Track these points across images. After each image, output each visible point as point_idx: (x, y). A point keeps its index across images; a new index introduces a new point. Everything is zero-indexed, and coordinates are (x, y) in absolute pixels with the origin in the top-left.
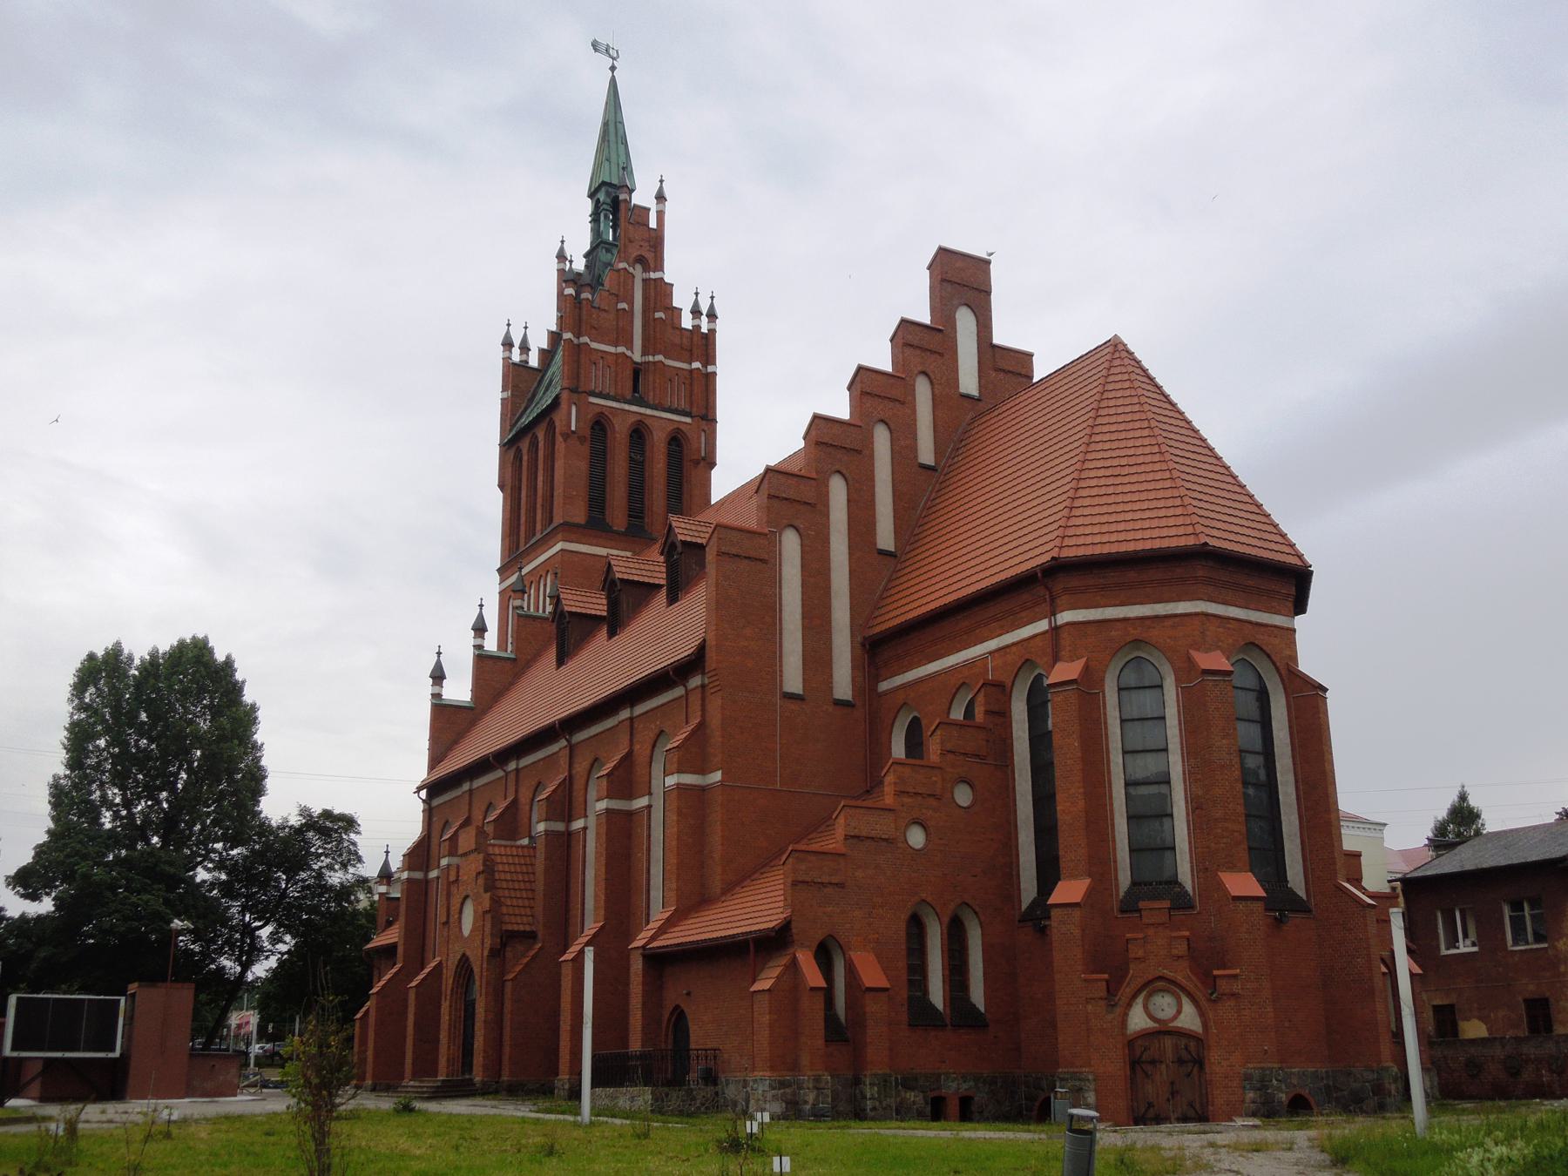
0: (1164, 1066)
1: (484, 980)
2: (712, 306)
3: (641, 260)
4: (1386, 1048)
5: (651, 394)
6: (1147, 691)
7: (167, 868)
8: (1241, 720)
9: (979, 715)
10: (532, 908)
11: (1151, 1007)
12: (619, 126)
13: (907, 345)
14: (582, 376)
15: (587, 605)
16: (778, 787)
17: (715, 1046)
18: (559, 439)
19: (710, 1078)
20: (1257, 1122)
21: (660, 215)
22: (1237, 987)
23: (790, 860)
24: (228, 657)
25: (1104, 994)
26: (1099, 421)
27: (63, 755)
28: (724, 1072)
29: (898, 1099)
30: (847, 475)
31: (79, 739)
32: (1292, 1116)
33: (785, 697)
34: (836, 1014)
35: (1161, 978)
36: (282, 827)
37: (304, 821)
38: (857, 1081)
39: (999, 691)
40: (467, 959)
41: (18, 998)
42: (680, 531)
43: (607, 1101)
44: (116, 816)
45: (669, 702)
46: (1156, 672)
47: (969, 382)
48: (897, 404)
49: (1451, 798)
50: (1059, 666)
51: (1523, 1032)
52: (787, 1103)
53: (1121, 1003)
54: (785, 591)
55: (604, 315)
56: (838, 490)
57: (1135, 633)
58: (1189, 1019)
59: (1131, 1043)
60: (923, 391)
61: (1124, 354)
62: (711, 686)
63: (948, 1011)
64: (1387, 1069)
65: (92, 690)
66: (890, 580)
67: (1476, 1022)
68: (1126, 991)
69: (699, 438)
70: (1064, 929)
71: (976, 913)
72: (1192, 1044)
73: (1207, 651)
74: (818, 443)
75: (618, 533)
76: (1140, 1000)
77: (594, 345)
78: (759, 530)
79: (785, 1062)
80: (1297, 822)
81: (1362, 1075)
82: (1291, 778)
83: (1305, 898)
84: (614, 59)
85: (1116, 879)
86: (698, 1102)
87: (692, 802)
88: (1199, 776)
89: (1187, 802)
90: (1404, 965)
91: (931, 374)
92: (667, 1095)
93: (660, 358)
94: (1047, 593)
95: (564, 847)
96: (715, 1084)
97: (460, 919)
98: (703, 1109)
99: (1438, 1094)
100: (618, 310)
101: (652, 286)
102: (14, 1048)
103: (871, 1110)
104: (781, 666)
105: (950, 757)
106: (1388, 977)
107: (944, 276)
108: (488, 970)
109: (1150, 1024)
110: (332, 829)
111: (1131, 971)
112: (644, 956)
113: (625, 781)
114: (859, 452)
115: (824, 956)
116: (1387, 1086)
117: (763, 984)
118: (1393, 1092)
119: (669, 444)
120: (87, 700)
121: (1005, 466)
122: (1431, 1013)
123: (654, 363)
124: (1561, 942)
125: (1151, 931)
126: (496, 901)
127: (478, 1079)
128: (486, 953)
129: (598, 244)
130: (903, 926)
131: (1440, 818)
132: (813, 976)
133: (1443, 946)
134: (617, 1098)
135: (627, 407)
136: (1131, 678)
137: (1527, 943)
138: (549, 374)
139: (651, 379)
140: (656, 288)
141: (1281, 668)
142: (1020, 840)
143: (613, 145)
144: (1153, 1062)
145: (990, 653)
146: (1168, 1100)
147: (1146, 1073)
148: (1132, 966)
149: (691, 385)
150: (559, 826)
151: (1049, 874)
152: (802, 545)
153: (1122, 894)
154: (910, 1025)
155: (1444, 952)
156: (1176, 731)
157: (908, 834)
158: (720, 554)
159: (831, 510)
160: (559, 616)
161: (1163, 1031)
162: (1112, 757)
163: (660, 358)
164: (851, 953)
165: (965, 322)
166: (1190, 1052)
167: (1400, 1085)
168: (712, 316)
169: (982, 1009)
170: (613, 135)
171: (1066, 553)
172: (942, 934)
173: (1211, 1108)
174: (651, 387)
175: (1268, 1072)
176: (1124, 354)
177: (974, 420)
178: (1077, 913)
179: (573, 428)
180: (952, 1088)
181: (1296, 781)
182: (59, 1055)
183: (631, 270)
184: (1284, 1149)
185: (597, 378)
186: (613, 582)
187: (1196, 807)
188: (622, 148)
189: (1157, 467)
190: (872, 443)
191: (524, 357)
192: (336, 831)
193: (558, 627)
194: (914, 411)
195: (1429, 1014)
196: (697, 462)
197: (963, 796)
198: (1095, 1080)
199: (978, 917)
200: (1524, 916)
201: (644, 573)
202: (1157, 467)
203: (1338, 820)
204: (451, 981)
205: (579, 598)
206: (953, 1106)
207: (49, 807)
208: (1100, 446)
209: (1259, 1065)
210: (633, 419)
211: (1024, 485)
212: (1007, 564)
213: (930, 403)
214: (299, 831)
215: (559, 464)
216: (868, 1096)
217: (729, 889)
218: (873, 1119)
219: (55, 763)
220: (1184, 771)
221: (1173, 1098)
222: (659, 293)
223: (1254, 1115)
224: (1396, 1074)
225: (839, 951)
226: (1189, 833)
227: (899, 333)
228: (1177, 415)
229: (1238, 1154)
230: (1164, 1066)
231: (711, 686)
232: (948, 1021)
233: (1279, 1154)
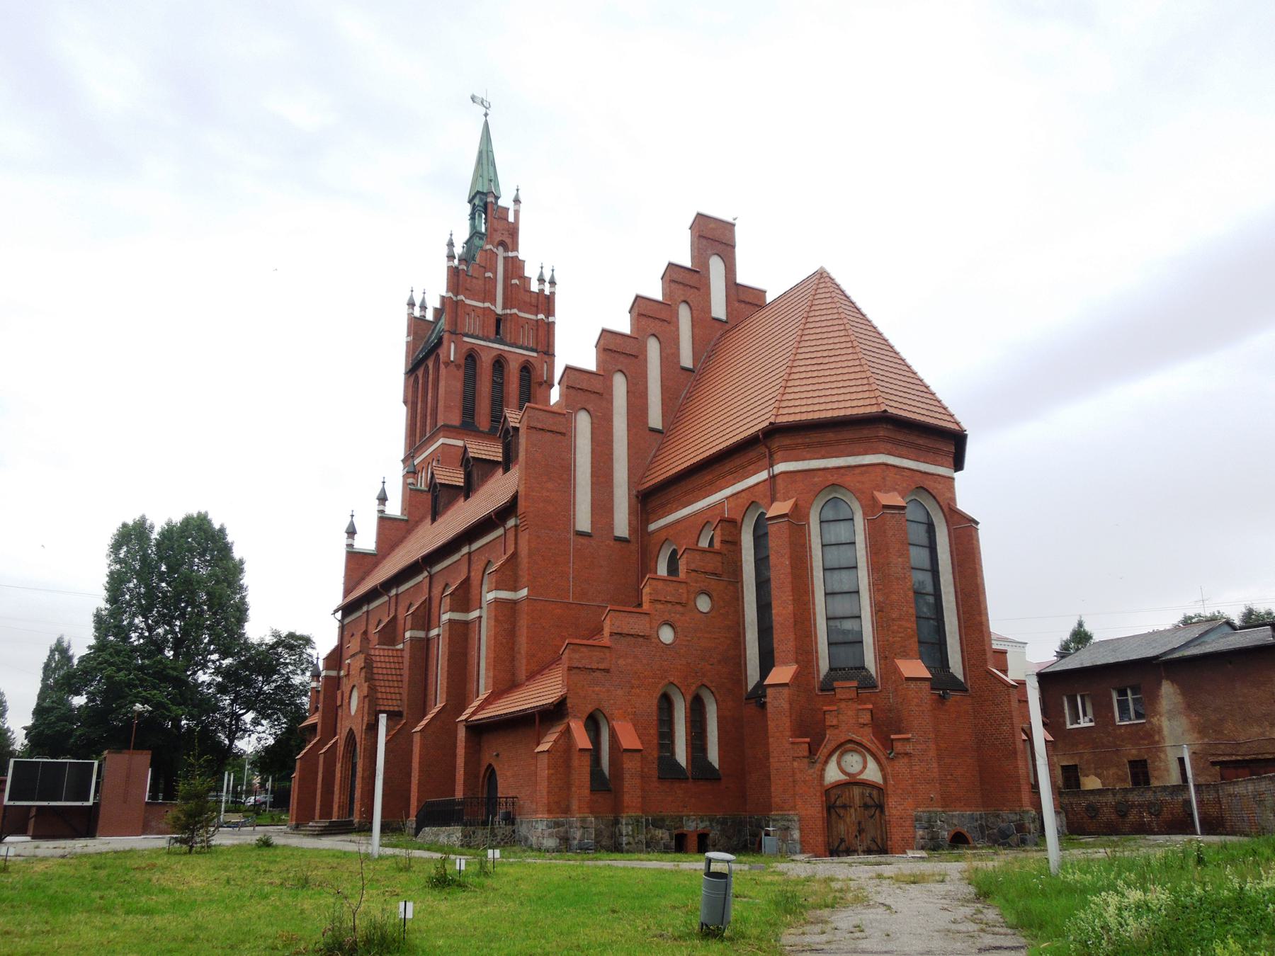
0: (853, 810)
1: (363, 747)
2: (553, 276)
3: (502, 244)
4: (1026, 797)
5: (508, 336)
6: (842, 523)
7: (171, 672)
8: (914, 545)
9: (717, 545)
10: (400, 694)
11: (843, 764)
12: (490, 153)
13: (673, 281)
14: (459, 323)
15: (453, 479)
16: (571, 601)
17: (514, 795)
18: (442, 366)
19: (510, 819)
20: (923, 854)
21: (517, 213)
22: (909, 748)
23: (567, 651)
24: (222, 526)
25: (806, 754)
26: (808, 326)
27: (105, 594)
28: (520, 815)
29: (649, 836)
30: (627, 373)
31: (116, 584)
32: (953, 849)
33: (577, 534)
34: (602, 770)
35: (850, 741)
36: (260, 645)
37: (275, 640)
38: (616, 822)
39: (731, 526)
40: (353, 732)
41: (15, 762)
42: (512, 420)
43: (432, 837)
44: (141, 636)
45: (494, 540)
46: (849, 509)
47: (719, 309)
48: (666, 324)
49: (1073, 625)
50: (776, 505)
51: (1129, 785)
52: (560, 839)
53: (819, 760)
54: (578, 456)
55: (474, 280)
56: (620, 385)
57: (833, 479)
58: (872, 773)
59: (828, 791)
60: (684, 315)
61: (827, 280)
62: (522, 525)
63: (690, 768)
64: (1027, 812)
65: (125, 549)
66: (658, 450)
67: (1093, 777)
68: (824, 751)
69: (542, 367)
70: (777, 703)
71: (712, 693)
72: (875, 793)
73: (887, 492)
74: (605, 350)
75: (482, 432)
76: (834, 758)
77: (468, 302)
78: (559, 411)
79: (559, 806)
80: (957, 623)
81: (262, 785)
82: (952, 590)
83: (963, 680)
84: (486, 108)
85: (818, 665)
86: (499, 838)
87: (506, 610)
88: (881, 587)
89: (871, 606)
90: (1040, 735)
91: (690, 302)
92: (474, 833)
93: (515, 311)
94: (767, 450)
95: (423, 648)
96: (513, 824)
97: (349, 702)
98: (502, 844)
99: (1066, 831)
100: (485, 278)
101: (510, 262)
102: (10, 799)
103: (626, 844)
104: (574, 511)
105: (694, 574)
106: (1028, 743)
107: (701, 233)
108: (365, 739)
109: (843, 777)
110: (296, 646)
111: (827, 736)
112: (467, 727)
113: (464, 598)
114: (636, 357)
115: (593, 723)
116: (1027, 825)
117: (544, 747)
118: (1032, 830)
119: (521, 371)
120: (122, 556)
121: (741, 364)
122: (1060, 772)
123: (511, 314)
124: (1156, 719)
125: (843, 705)
126: (372, 689)
127: (356, 820)
128: (364, 728)
129: (475, 233)
130: (655, 702)
131: (1065, 639)
132: (582, 739)
133: (1068, 722)
134: (438, 835)
135: (491, 345)
136: (829, 514)
137: (1130, 719)
138: (440, 324)
139: (508, 326)
140: (513, 263)
141: (943, 507)
142: (747, 638)
143: (485, 167)
144: (844, 807)
145: (727, 498)
146: (856, 836)
147: (839, 815)
148: (828, 732)
149: (537, 330)
150: (421, 634)
151: (767, 664)
152: (592, 423)
153: (822, 677)
154: (659, 778)
155: (1069, 726)
156: (864, 552)
157: (660, 632)
158: (529, 428)
159: (614, 397)
160: (434, 487)
161: (853, 783)
162: (815, 573)
163: (515, 311)
164: (614, 723)
165: (716, 267)
166: (873, 799)
167: (1037, 824)
168: (553, 283)
169: (717, 766)
170: (485, 159)
171: (781, 420)
172: (686, 709)
173: (889, 843)
174: (508, 331)
175: (933, 815)
176: (827, 280)
177: (722, 336)
178: (785, 691)
179: (452, 359)
180: (692, 826)
181: (956, 592)
182: (45, 803)
183: (495, 250)
184: (938, 882)
185: (470, 324)
186: (468, 460)
187: (879, 610)
188: (491, 169)
189: (850, 357)
190: (646, 351)
191: (423, 313)
192: (299, 647)
193: (433, 495)
194: (678, 329)
195: (1059, 772)
196: (540, 384)
197: (704, 604)
198: (799, 821)
199: (714, 696)
200: (1127, 700)
201: (491, 453)
202: (850, 357)
203: (990, 640)
204: (342, 748)
205: (448, 474)
206: (693, 842)
207: (94, 630)
208: (808, 343)
209: (927, 809)
210: (495, 353)
211: (753, 375)
212: (741, 429)
213: (690, 323)
214: (273, 647)
215: (442, 384)
216: (624, 833)
217: (532, 676)
218: (628, 851)
219: (99, 599)
220: (869, 583)
221: (860, 834)
222: (515, 267)
223: (923, 848)
224: (1035, 815)
225: (605, 722)
226: (873, 630)
227: (668, 273)
228: (866, 323)
229: (897, 885)
230: (853, 810)
231: (522, 525)
232: (689, 775)
233: (932, 886)
